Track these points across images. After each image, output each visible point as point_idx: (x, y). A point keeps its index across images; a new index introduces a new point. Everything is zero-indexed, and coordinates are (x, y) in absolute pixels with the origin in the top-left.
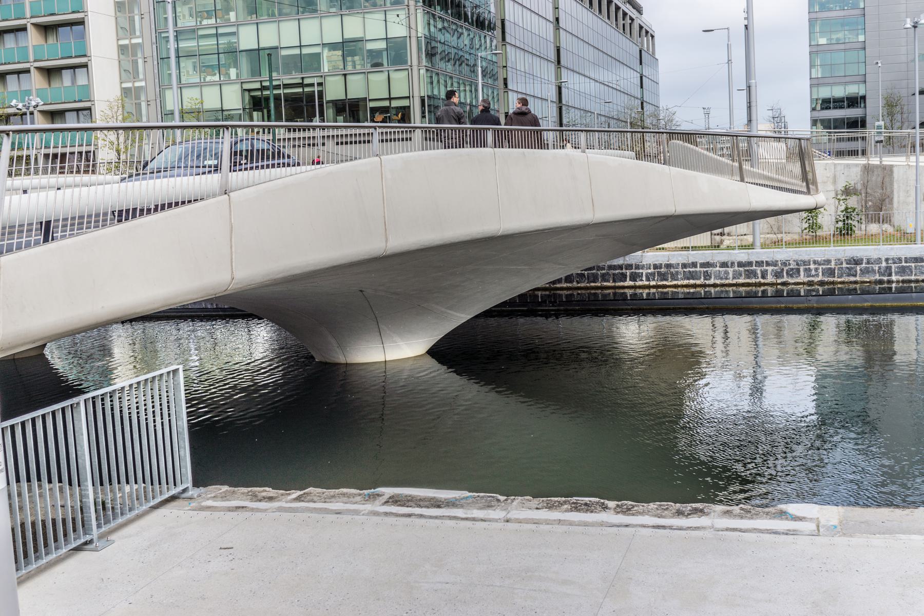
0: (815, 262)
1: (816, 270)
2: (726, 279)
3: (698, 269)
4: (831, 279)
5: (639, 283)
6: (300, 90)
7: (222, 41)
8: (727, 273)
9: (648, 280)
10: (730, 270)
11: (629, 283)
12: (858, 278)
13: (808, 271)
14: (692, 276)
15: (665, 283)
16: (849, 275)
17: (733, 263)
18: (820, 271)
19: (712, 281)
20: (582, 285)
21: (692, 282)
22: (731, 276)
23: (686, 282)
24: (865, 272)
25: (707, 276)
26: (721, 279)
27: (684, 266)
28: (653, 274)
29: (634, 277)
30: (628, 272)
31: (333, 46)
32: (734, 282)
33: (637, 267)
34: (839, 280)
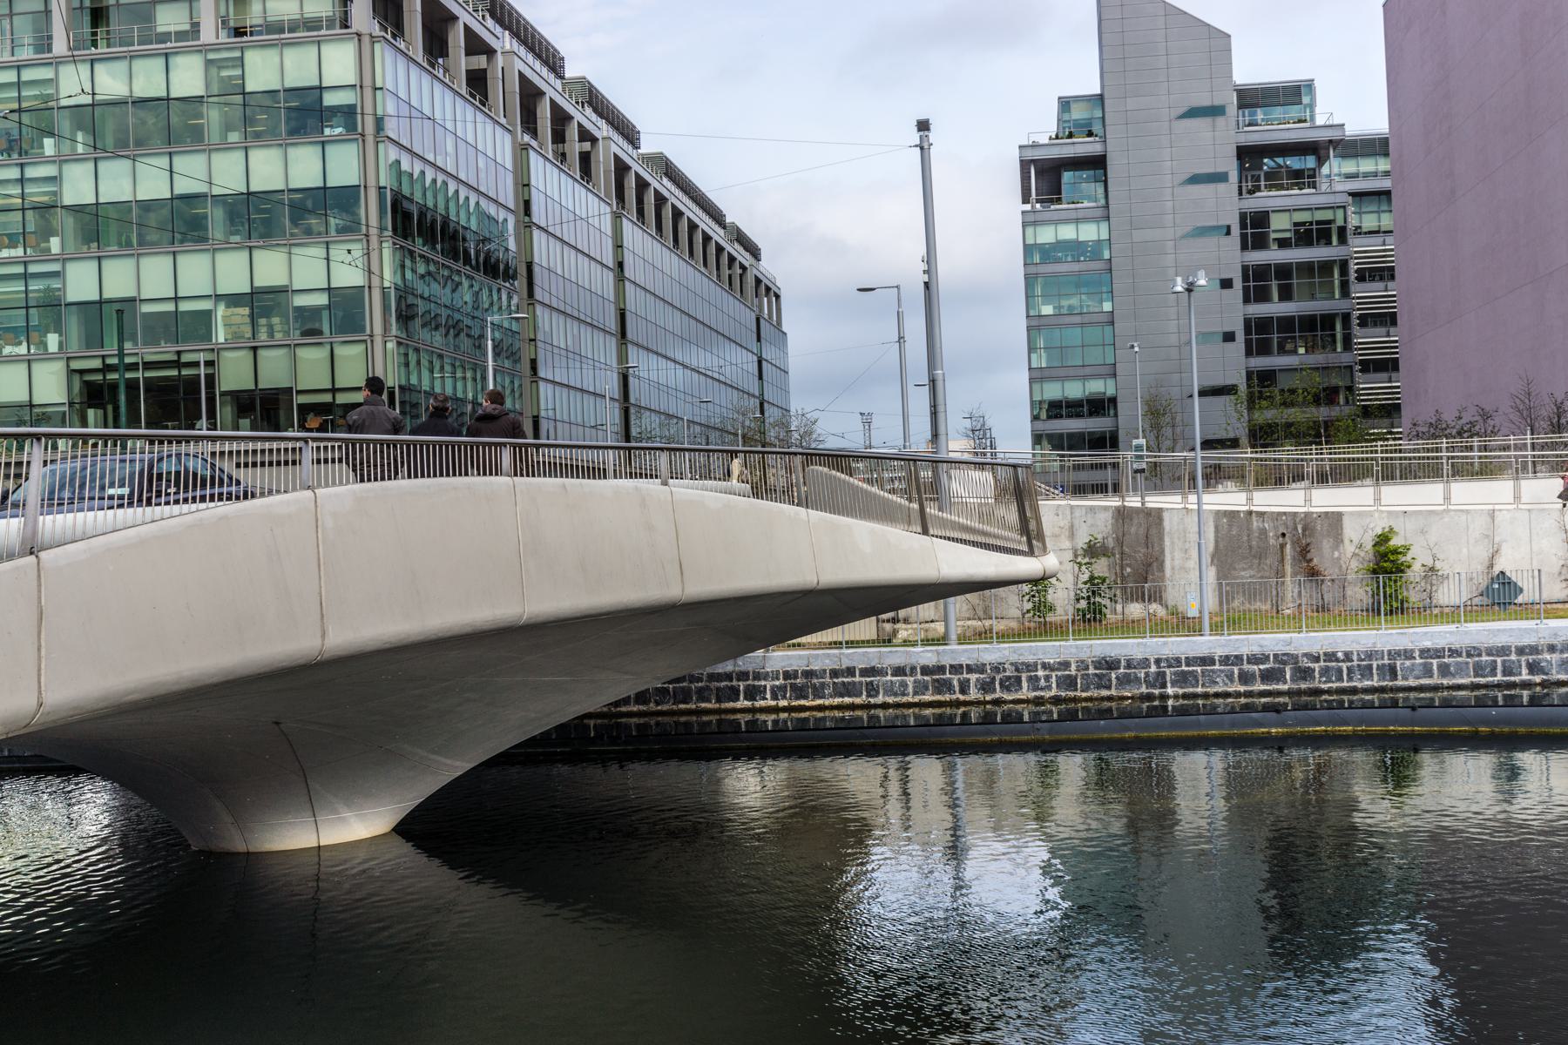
0: (1045, 666)
1: (1047, 678)
2: (904, 694)
3: (857, 679)
4: (1072, 694)
5: (760, 703)
6: (174, 373)
7: (34, 286)
8: (904, 685)
9: (775, 697)
10: (910, 680)
11: (743, 703)
12: (1113, 692)
13: (1034, 680)
14: (848, 690)
15: (803, 702)
16: (1099, 687)
17: (913, 669)
18: (1054, 680)
19: (880, 699)
20: (665, 707)
21: (847, 700)
22: (910, 689)
23: (837, 701)
24: (1124, 681)
25: (872, 690)
26: (896, 695)
27: (835, 673)
28: (783, 688)
29: (752, 693)
30: (742, 685)
31: (233, 300)
32: (916, 699)
33: (757, 676)
34: (1084, 695)
